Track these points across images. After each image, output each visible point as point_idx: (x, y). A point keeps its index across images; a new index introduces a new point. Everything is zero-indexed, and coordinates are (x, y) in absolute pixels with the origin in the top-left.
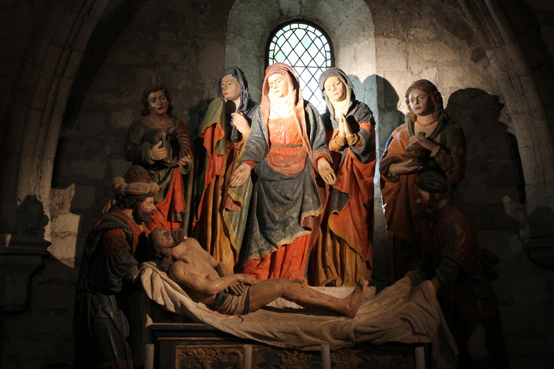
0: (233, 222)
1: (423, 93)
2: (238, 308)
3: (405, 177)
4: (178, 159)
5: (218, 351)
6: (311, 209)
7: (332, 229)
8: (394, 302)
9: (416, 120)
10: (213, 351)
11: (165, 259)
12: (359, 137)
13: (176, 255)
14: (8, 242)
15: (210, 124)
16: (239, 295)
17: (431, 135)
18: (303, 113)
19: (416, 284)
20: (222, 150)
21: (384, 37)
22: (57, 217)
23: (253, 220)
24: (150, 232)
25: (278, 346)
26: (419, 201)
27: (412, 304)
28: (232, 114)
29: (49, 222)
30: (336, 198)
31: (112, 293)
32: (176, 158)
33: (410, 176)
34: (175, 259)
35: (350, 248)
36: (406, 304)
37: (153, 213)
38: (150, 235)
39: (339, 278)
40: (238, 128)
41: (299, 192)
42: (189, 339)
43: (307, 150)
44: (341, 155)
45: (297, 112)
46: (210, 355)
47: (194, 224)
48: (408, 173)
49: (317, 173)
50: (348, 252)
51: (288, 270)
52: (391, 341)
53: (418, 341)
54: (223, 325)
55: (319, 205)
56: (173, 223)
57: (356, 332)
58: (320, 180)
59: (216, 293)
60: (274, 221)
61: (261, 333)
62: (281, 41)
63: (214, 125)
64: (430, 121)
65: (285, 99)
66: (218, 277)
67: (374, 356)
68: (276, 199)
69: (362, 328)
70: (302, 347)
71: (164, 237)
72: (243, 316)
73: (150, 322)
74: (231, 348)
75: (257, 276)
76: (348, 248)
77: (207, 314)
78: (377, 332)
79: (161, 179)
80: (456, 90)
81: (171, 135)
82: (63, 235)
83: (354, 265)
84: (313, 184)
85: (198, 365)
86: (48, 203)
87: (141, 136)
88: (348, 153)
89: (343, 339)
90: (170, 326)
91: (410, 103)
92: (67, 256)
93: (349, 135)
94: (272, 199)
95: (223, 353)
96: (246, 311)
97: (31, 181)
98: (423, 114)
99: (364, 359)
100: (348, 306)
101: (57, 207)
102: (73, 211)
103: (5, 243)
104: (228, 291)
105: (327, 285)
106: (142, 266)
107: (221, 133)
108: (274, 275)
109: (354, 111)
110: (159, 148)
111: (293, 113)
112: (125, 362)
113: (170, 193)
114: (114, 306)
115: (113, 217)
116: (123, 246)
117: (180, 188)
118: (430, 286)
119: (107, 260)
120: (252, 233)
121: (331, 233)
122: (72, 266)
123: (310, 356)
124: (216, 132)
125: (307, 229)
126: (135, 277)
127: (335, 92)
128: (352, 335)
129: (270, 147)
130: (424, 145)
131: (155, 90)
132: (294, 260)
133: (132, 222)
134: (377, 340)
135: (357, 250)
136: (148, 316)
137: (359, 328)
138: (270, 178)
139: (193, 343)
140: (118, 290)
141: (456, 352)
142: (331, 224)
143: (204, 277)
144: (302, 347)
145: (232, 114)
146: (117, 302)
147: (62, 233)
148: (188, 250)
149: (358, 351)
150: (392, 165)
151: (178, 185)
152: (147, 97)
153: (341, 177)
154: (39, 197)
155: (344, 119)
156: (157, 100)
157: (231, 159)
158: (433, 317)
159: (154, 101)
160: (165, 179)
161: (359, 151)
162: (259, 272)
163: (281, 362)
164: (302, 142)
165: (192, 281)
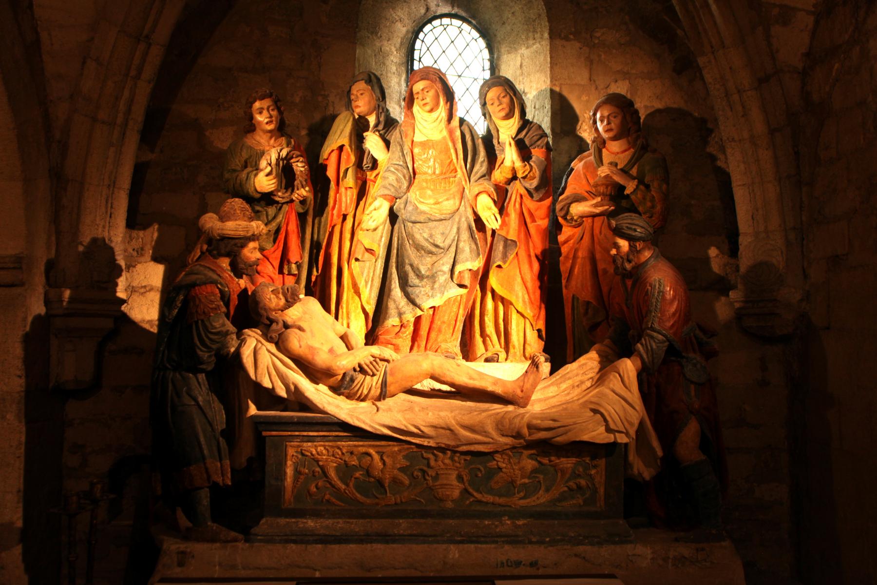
0: (363, 276)
1: (616, 110)
2: (372, 392)
3: (590, 220)
4: (293, 191)
5: (344, 451)
6: (467, 260)
7: (494, 287)
8: (578, 386)
9: (604, 147)
10: (338, 451)
11: (274, 326)
12: (531, 167)
13: (289, 321)
14: (66, 300)
15: (335, 146)
16: (374, 375)
17: (625, 166)
18: (458, 133)
19: (607, 363)
20: (350, 180)
21: (562, 39)
22: (134, 267)
23: (391, 274)
24: (254, 288)
25: (426, 444)
26: (614, 252)
27: (604, 389)
28: (365, 134)
29: (124, 274)
30: (500, 247)
31: (202, 371)
32: (290, 190)
33: (596, 219)
34: (286, 326)
35: (518, 312)
36: (597, 390)
37: (257, 263)
38: (254, 292)
39: (503, 350)
40: (372, 152)
41: (452, 238)
42: (305, 434)
43: (464, 183)
44: (507, 191)
45: (451, 133)
46: (333, 455)
47: (313, 279)
48: (594, 216)
49: (475, 214)
50: (514, 317)
51: (436, 340)
52: (578, 440)
53: (612, 440)
54: (351, 416)
55: (479, 255)
56: (286, 277)
57: (530, 427)
58: (479, 224)
59: (342, 372)
60: (420, 276)
61: (403, 427)
62: (429, 39)
63: (341, 148)
64: (624, 148)
65: (435, 115)
66: (346, 350)
67: (553, 458)
68: (423, 248)
69: (539, 422)
70: (458, 446)
71: (273, 296)
72: (378, 404)
73: (253, 410)
74: (362, 446)
75: (397, 349)
76: (514, 312)
77: (331, 400)
78: (559, 427)
79: (270, 218)
80: (653, 110)
81: (283, 159)
82: (143, 290)
83: (522, 335)
84: (470, 228)
85: (318, 469)
86: (122, 248)
87: (243, 160)
88: (516, 189)
89: (512, 436)
90: (280, 417)
91: (599, 123)
92: (148, 318)
93: (518, 164)
94: (418, 247)
95: (352, 453)
96: (382, 396)
97: (98, 218)
98: (614, 139)
99: (540, 462)
100: (519, 392)
101: (135, 254)
102: (156, 259)
103: (62, 301)
104: (358, 369)
105: (487, 360)
106: (243, 334)
107: (349, 158)
108: (419, 346)
109: (524, 133)
110: (267, 175)
111: (445, 133)
112: (219, 464)
113: (282, 236)
114: (204, 389)
115: (202, 268)
116: (216, 309)
117: (296, 230)
118: (629, 367)
119: (194, 327)
120: (390, 290)
121: (493, 292)
122: (155, 330)
123: (468, 458)
124: (344, 156)
125: (461, 286)
126: (233, 350)
127: (500, 107)
128: (525, 431)
129: (414, 178)
130: (617, 178)
131: (262, 98)
132: (444, 326)
133: (25, 319)
134: (558, 439)
135: (525, 315)
136: (250, 402)
137: (535, 422)
138: (413, 218)
139: (310, 439)
140: (210, 368)
141: (660, 453)
142: (493, 281)
143: (327, 350)
144: (458, 446)
145: (365, 134)
146: (209, 384)
147: (142, 287)
148: (305, 313)
149: (532, 452)
150: (573, 205)
151: (293, 226)
152: (251, 107)
153: (507, 219)
154: (110, 239)
155: (513, 143)
156: (265, 112)
157: (362, 193)
158: (634, 408)
159: (261, 113)
160: (275, 217)
161: (531, 185)
162: (398, 341)
163: (429, 466)
164: (456, 171)
165: (310, 357)
